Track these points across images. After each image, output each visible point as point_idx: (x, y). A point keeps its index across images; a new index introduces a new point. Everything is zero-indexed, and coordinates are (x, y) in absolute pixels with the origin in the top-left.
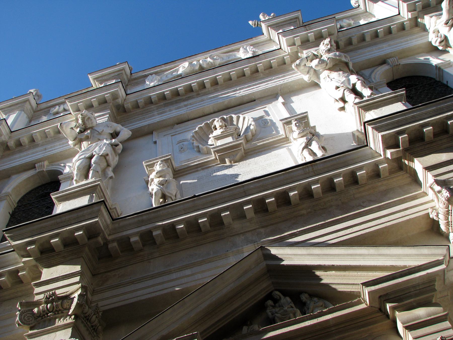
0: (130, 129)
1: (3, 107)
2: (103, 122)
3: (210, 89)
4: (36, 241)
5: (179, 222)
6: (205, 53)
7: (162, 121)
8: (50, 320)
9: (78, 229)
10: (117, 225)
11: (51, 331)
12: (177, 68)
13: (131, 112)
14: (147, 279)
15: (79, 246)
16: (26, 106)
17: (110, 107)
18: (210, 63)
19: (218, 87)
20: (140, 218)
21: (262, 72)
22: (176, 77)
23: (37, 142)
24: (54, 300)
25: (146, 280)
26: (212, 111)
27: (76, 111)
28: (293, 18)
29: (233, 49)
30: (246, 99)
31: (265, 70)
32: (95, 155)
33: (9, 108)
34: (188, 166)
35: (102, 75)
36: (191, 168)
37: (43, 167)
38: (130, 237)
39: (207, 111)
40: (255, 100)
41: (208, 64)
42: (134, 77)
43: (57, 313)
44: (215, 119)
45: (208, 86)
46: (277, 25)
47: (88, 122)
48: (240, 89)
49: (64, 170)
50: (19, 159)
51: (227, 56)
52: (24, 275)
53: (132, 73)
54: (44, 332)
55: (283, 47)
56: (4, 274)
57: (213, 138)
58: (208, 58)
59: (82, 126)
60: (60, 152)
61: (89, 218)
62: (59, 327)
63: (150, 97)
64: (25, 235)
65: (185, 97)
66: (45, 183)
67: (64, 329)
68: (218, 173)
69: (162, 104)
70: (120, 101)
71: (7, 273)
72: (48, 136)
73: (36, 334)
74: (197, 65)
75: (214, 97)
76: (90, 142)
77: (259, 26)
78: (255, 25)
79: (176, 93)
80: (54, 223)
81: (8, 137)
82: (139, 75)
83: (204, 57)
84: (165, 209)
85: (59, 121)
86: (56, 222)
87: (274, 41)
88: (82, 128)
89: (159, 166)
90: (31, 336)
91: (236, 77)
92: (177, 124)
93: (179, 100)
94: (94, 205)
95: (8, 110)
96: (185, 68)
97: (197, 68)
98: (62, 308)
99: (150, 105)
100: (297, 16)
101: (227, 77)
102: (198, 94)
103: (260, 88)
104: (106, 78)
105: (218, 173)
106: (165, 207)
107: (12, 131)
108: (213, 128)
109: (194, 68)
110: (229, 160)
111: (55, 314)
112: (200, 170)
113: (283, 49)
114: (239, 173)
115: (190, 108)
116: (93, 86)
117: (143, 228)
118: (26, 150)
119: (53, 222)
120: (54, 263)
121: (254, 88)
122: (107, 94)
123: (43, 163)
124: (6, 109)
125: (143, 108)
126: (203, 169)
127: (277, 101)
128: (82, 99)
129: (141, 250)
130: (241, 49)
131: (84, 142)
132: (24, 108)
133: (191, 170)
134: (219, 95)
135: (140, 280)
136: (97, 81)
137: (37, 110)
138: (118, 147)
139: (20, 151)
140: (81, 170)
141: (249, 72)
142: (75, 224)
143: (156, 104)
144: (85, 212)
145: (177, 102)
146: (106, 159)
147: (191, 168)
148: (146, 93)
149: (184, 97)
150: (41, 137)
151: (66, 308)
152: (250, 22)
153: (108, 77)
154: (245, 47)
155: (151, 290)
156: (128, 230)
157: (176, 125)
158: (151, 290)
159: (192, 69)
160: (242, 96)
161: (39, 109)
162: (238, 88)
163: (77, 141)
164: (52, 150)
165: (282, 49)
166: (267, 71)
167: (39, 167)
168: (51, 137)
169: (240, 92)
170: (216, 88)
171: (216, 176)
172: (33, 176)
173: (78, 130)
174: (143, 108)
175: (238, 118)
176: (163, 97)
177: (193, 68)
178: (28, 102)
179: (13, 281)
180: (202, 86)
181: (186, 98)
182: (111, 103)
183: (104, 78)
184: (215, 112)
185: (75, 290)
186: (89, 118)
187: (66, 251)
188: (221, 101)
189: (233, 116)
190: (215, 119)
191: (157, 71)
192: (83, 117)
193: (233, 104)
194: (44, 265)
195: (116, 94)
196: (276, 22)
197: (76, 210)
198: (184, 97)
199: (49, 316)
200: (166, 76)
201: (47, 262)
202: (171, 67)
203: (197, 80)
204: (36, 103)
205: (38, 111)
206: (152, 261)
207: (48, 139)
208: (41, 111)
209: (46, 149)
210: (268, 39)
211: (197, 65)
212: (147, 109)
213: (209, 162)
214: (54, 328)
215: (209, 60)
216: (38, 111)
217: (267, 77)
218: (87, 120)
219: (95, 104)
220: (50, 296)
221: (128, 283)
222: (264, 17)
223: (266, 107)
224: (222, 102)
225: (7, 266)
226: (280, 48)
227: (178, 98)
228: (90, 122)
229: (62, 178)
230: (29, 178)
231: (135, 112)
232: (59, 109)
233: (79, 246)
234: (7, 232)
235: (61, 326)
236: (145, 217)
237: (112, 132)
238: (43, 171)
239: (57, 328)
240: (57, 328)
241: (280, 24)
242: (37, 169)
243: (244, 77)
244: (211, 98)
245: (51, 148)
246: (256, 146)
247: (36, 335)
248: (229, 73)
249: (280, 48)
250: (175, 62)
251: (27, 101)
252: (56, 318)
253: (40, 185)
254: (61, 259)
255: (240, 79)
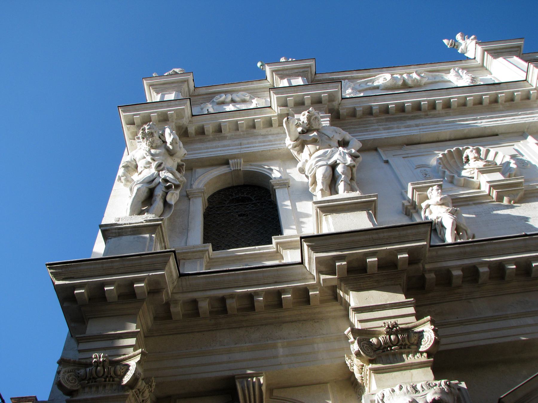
0: (358, 139)
1: (155, 83)
2: (327, 126)
3: (441, 112)
4: (346, 256)
5: (510, 261)
6: (406, 67)
7: (391, 138)
8: (394, 355)
9: (401, 251)
10: (434, 253)
11: (403, 368)
12: (373, 78)
13: (345, 120)
14: (479, 322)
15: (397, 271)
16: (184, 87)
17: (325, 108)
18: (415, 81)
19: (451, 111)
20: (462, 250)
21: (501, 104)
22: (372, 88)
23: (224, 134)
24: (398, 331)
25: (477, 322)
26: (448, 138)
27: (281, 105)
28: (514, 45)
29: (439, 69)
30: (488, 132)
31: (505, 102)
32: (339, 164)
33: (162, 86)
34: (456, 197)
35: (283, 68)
36: (460, 200)
37: (239, 166)
38: (451, 270)
39: (442, 137)
40: (497, 135)
41: (413, 80)
42: (319, 78)
43: (403, 348)
44: (469, 147)
45: (439, 107)
46: (496, 51)
47: (315, 122)
48: (481, 119)
49: (271, 174)
50: (205, 151)
51: (432, 76)
52: (316, 295)
53: (316, 73)
54: (394, 368)
55: (529, 80)
56: (288, 290)
57: (477, 170)
58: (413, 73)
59: (307, 125)
60: (262, 151)
61: (414, 239)
62: (413, 364)
63: (371, 108)
64: (331, 248)
65: (412, 115)
66: (236, 185)
67: (420, 368)
68: (500, 212)
69: (384, 117)
70: (335, 104)
71: (292, 290)
72: (239, 129)
73: (384, 369)
74: (401, 79)
75: (450, 122)
76: (318, 147)
77: (455, 47)
78: (451, 45)
79: (401, 109)
80: (370, 238)
81: (188, 121)
82: (326, 77)
83: (408, 71)
84: (491, 244)
85: (255, 113)
86: (372, 238)
87: (486, 69)
88: (305, 128)
89: (437, 192)
90: (378, 371)
91: (472, 104)
92: (407, 145)
93: (404, 117)
94: (420, 225)
95: (161, 88)
96: (386, 80)
97: (400, 83)
98: (409, 342)
99: (369, 116)
100: (520, 45)
101: (462, 101)
102: (427, 115)
103: (504, 121)
104: (287, 72)
105: (500, 212)
106: (492, 241)
107: (193, 114)
108: (465, 158)
109: (396, 82)
110: (508, 198)
111: (401, 348)
112: (471, 205)
113: (530, 82)
114: (529, 217)
115: (423, 129)
116: (267, 79)
117: (467, 262)
118: (209, 141)
119: (367, 237)
120: (363, 287)
121: (498, 121)
122: (324, 93)
123: (238, 160)
124: (158, 87)
125: (361, 118)
126: (475, 204)
127: (525, 140)
128: (291, 92)
129: (459, 287)
130: (452, 71)
131: (309, 146)
132: (181, 90)
133: (459, 202)
134: (456, 121)
135: (472, 321)
136: (276, 74)
137: (195, 94)
138: (358, 158)
139: (201, 141)
140: (327, 178)
141: (488, 101)
142: (396, 244)
143: (377, 116)
144: (409, 231)
145: (401, 119)
146: (352, 171)
147: (460, 200)
148: (366, 101)
149: (410, 115)
150: (230, 129)
151: (413, 343)
152: (445, 41)
153: (290, 72)
154: (456, 70)
155: (488, 335)
156: (447, 261)
157: (405, 146)
158: (488, 335)
159: (394, 83)
160: (485, 127)
161: (196, 94)
162: (478, 117)
163: (298, 142)
164: (251, 147)
165: (528, 82)
166: (508, 104)
167: (234, 165)
168: (242, 131)
169: (482, 122)
170: (447, 112)
171: (497, 214)
172: (225, 174)
173: (300, 129)
174: (361, 118)
175: (488, 151)
176: (385, 110)
177: (395, 81)
178: (186, 83)
179: (294, 300)
180: (433, 106)
181: (413, 116)
182: (326, 104)
183: (285, 72)
184: (450, 140)
185: (421, 323)
186: (316, 118)
187: (381, 274)
188: (460, 128)
189: (481, 148)
190: (469, 147)
191: (348, 77)
192: (309, 116)
193: (472, 134)
194: (351, 287)
195: (333, 95)
196: (493, 48)
197: (398, 228)
198: (410, 115)
199: (392, 350)
200: (360, 85)
201: (355, 284)
202: (364, 76)
203: (428, 99)
204: (194, 85)
205: (195, 96)
206: (472, 301)
207: (238, 133)
208: (199, 97)
209: (241, 144)
210: (479, 65)
211: (400, 79)
212: (365, 121)
213: (481, 198)
214: (407, 365)
215: (414, 76)
216: (195, 96)
217: (507, 110)
218: (313, 120)
219: (307, 102)
220: (393, 326)
221: (457, 323)
222: (463, 38)
223: (514, 145)
224: (462, 129)
225: (291, 281)
226: (525, 79)
227: (403, 115)
228: (317, 122)
229: (276, 183)
230: (221, 175)
231: (350, 121)
232: (226, 98)
233: (397, 271)
234: (307, 239)
235: (417, 364)
236: (468, 249)
237: (340, 140)
238: (240, 170)
239: (411, 366)
240: (411, 366)
241: (499, 51)
242: (231, 166)
243: (480, 106)
244: (447, 122)
245: (248, 143)
246: (534, 188)
247: (385, 370)
248: (466, 97)
249: (526, 80)
250: (369, 70)
251: (185, 81)
252: (402, 354)
253: (230, 186)
254: (373, 283)
255: (476, 106)
